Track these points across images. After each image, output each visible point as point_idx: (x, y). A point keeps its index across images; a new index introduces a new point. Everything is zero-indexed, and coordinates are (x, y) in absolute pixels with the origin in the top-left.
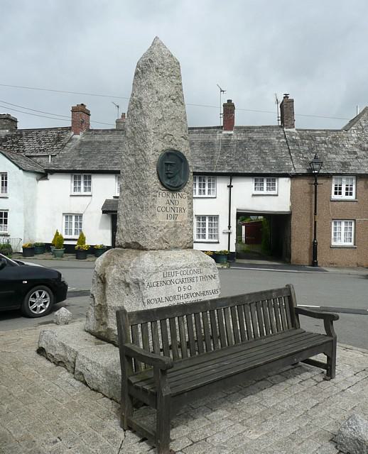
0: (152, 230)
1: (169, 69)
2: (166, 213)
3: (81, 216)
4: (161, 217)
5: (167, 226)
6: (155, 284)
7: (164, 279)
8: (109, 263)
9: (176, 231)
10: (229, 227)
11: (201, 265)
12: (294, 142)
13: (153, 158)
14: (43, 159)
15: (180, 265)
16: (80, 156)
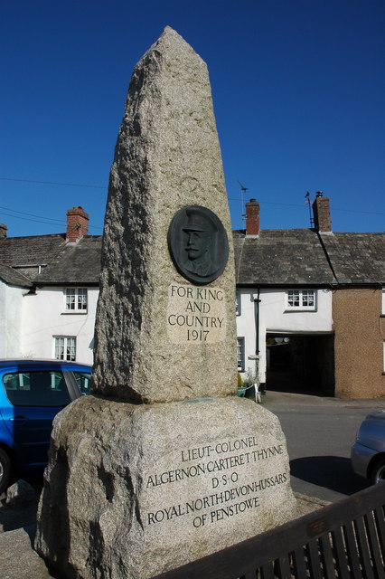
0: (159, 363)
1: (190, 70)
2: (185, 328)
3: (74, 338)
4: (176, 335)
5: (188, 354)
6: (165, 478)
7: (185, 466)
8: (76, 426)
9: (205, 364)
10: (257, 352)
11: (255, 429)
12: (334, 247)
13: (160, 220)
14: (31, 270)
15: (214, 431)
16: (75, 266)
